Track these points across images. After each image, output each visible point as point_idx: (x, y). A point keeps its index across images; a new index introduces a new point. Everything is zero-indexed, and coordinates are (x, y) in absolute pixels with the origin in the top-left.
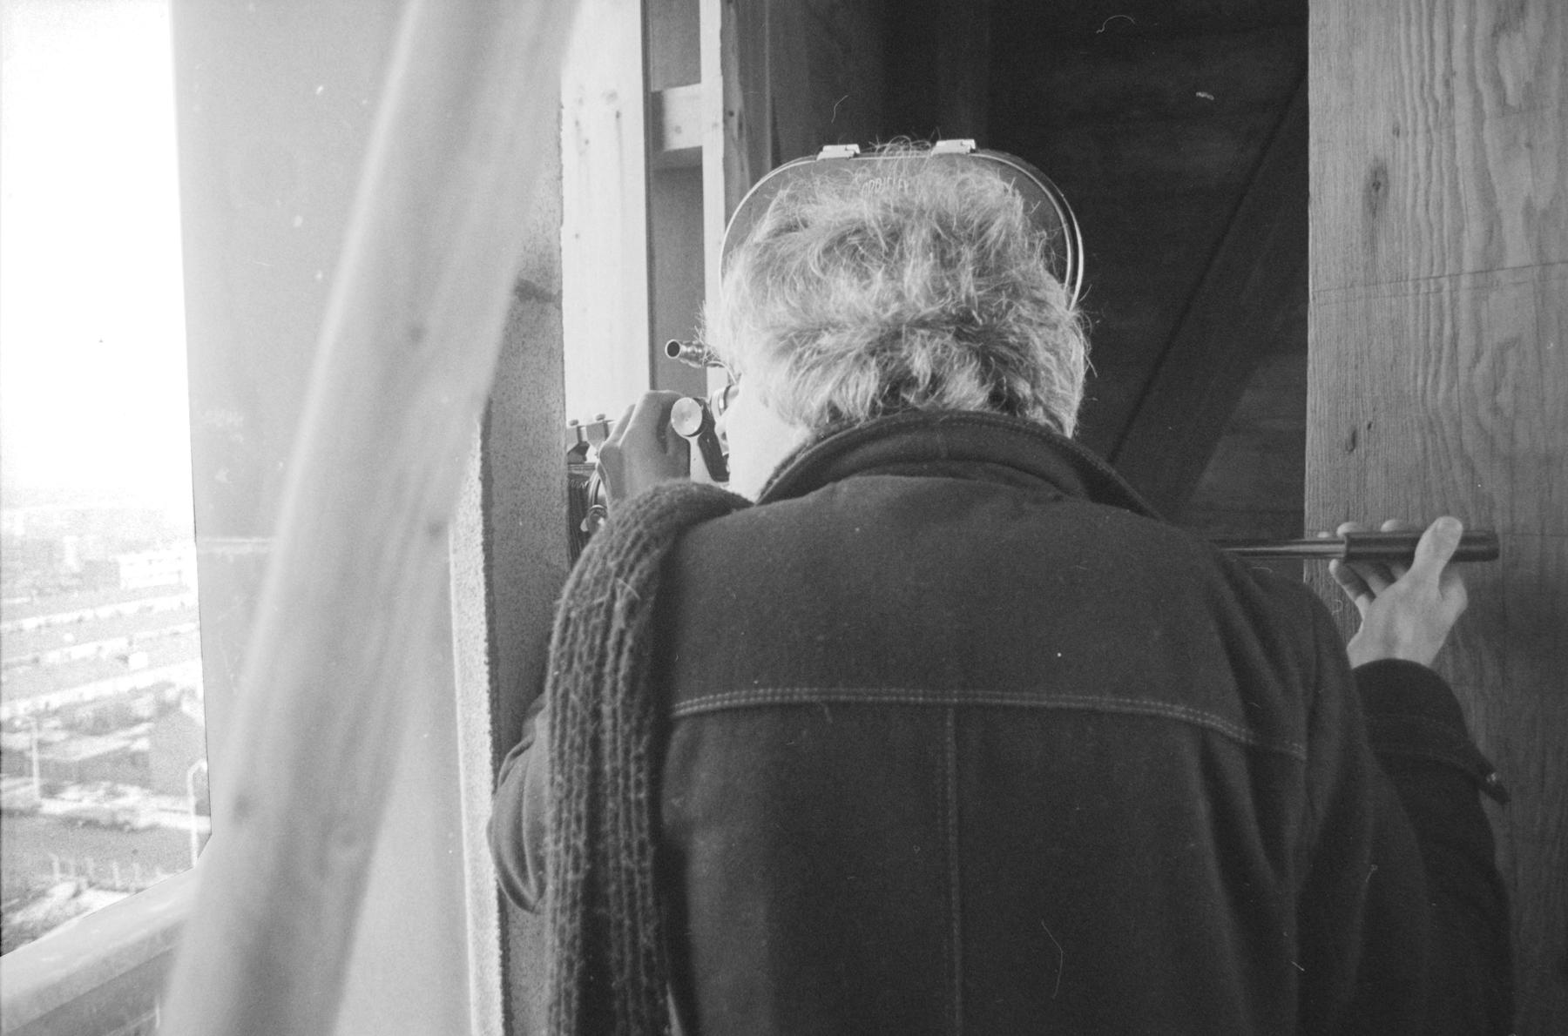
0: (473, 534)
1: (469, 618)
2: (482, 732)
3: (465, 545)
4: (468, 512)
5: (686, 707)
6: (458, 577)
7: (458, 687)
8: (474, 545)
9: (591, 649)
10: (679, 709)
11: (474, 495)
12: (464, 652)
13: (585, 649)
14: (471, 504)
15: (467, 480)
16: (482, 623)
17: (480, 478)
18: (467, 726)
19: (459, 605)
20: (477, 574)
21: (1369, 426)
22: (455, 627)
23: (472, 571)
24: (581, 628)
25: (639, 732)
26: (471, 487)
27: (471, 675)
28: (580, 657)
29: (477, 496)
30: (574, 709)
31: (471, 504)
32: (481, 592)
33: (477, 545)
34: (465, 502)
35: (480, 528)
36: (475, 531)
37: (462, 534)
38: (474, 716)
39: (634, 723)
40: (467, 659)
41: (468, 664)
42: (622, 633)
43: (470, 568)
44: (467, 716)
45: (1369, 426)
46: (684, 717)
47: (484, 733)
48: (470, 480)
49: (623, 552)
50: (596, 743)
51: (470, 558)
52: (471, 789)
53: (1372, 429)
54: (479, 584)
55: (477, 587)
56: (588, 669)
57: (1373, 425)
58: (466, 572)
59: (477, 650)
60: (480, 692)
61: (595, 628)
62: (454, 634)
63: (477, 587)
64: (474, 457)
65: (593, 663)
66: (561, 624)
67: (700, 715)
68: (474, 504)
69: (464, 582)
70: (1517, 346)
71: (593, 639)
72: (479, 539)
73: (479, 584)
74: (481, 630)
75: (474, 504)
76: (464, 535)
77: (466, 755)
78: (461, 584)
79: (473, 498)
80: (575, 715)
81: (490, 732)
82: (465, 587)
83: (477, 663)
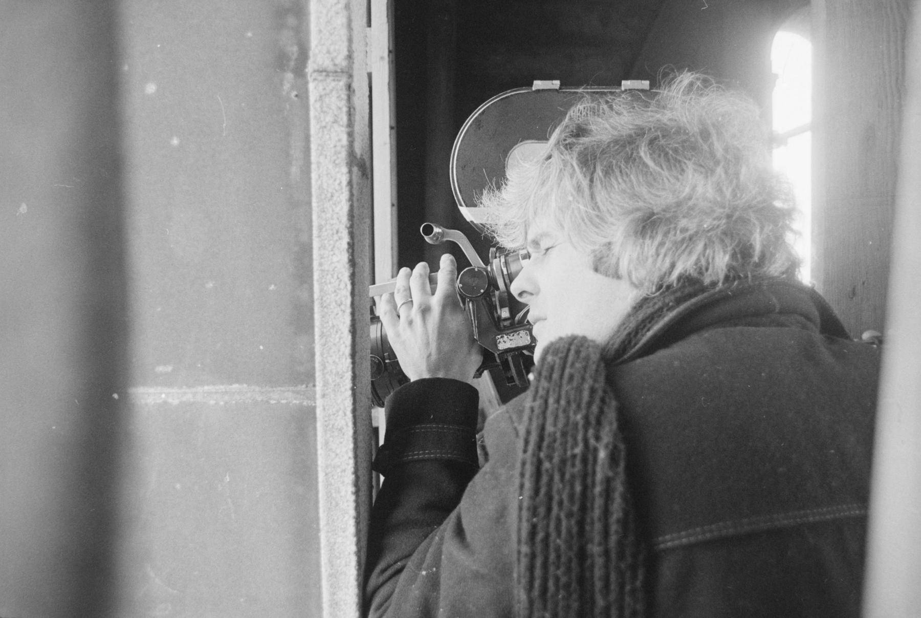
0: (342, 380)
1: (337, 455)
2: (347, 553)
3: (335, 391)
4: (337, 360)
5: (669, 540)
6: (326, 419)
7: (322, 514)
8: (343, 390)
9: (572, 496)
10: (665, 542)
11: (343, 346)
12: (331, 484)
13: (565, 497)
14: (341, 353)
15: (337, 332)
16: (350, 458)
17: (350, 331)
18: (331, 550)
19: (326, 443)
20: (345, 414)
21: (864, 283)
22: (321, 461)
23: (341, 413)
24: (557, 477)
25: (634, 568)
26: (340, 338)
27: (337, 504)
28: (561, 503)
29: (346, 346)
30: (557, 550)
31: (341, 353)
32: (350, 431)
33: (346, 390)
34: (334, 352)
35: (349, 375)
36: (344, 378)
37: (330, 381)
38: (340, 540)
39: (629, 560)
40: (333, 491)
41: (334, 495)
42: (608, 481)
43: (338, 411)
44: (332, 540)
45: (864, 283)
46: (673, 550)
47: (349, 554)
48: (339, 332)
49: (584, 405)
50: (583, 581)
51: (339, 402)
52: (334, 604)
53: (865, 284)
54: (347, 425)
55: (345, 427)
56: (570, 515)
57: (865, 283)
58: (334, 414)
59: (343, 482)
60: (346, 519)
61: (573, 476)
62: (320, 469)
63: (345, 427)
64: (344, 312)
65: (575, 508)
66: (531, 476)
67: (689, 547)
68: (343, 354)
69: (332, 422)
70: (526, 202)
71: (572, 486)
72: (348, 384)
73: (347, 425)
74: (348, 464)
75: (343, 354)
76: (333, 381)
77: (331, 575)
78: (328, 425)
79: (342, 348)
80: (558, 557)
81: (355, 553)
82: (333, 427)
83: (343, 493)
